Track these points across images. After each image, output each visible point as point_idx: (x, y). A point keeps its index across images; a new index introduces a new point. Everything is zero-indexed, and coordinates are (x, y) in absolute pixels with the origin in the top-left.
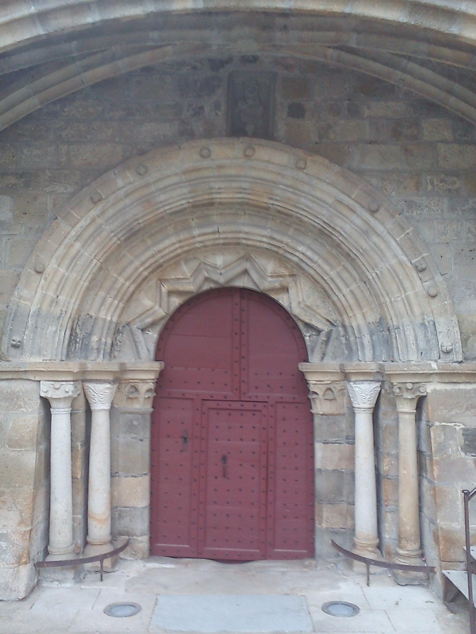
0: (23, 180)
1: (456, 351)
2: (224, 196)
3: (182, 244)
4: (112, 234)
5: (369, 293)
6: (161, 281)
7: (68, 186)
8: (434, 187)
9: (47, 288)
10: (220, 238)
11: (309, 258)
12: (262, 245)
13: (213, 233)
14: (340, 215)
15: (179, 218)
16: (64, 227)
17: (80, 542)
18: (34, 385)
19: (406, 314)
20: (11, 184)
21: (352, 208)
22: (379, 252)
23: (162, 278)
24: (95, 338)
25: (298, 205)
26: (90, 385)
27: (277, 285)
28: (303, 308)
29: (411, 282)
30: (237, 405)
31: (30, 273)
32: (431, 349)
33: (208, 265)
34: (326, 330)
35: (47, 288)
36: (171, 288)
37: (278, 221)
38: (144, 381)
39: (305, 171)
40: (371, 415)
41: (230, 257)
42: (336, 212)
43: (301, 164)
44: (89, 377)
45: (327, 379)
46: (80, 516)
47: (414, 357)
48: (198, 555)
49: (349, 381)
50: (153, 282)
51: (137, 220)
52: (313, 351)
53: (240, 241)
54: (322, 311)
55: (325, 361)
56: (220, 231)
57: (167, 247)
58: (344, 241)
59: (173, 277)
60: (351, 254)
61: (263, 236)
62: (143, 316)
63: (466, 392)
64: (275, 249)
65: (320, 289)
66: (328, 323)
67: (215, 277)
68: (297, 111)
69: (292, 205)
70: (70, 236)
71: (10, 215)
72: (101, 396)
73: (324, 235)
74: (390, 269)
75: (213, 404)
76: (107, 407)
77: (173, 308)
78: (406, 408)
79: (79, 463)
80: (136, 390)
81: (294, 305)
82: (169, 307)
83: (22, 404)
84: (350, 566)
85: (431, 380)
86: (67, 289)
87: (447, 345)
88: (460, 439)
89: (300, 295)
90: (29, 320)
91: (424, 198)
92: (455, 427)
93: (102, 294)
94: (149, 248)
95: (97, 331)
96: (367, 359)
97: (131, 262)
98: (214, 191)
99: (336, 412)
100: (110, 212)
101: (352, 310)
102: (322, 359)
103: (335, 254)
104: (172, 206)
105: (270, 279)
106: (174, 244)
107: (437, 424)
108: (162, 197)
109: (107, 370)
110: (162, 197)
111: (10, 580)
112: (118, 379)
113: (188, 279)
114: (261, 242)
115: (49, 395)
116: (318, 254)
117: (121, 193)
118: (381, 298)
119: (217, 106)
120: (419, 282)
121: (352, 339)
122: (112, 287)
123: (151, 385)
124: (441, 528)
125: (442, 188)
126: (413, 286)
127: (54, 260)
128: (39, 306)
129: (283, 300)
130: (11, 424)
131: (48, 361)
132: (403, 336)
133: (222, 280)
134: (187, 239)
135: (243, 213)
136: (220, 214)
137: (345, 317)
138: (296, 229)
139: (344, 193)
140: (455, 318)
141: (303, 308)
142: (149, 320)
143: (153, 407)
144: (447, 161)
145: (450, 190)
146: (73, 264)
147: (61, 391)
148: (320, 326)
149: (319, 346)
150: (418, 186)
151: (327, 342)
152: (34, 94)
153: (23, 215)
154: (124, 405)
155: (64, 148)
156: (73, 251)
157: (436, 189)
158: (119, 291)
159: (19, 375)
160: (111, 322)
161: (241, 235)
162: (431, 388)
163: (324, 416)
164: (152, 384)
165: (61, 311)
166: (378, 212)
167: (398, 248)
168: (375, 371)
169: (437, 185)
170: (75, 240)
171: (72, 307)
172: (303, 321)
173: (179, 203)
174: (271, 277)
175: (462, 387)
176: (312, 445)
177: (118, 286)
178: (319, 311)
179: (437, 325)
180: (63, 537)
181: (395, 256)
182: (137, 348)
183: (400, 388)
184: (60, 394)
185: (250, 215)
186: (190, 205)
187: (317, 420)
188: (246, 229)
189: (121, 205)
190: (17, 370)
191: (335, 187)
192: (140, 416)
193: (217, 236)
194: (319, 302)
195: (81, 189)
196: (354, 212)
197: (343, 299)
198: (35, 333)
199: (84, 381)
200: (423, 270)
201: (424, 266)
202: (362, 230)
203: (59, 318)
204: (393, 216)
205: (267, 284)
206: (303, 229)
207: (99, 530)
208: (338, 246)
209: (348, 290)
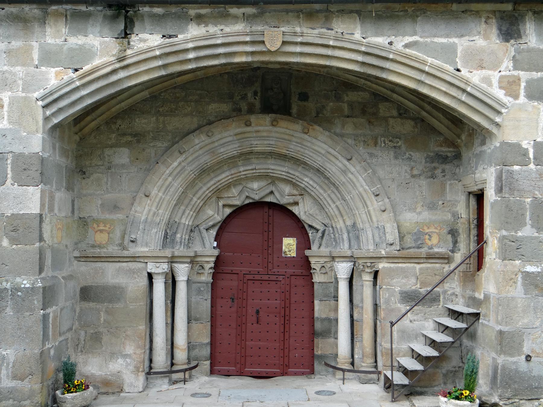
3: (233, 176)
6: (219, 198)
12: (282, 176)
13: (252, 170)
15: (231, 161)
16: (161, 168)
17: (169, 363)
18: (143, 265)
24: (179, 236)
26: (176, 265)
27: (291, 201)
29: (371, 202)
30: (266, 277)
32: (382, 243)
36: (225, 203)
38: (208, 262)
41: (263, 183)
45: (322, 260)
46: (170, 347)
47: (371, 247)
48: (241, 374)
49: (335, 262)
50: (214, 199)
52: (313, 243)
53: (269, 174)
54: (319, 217)
55: (322, 248)
57: (224, 178)
62: (207, 221)
63: (402, 268)
67: (253, 196)
68: (304, 97)
71: (128, 160)
72: (182, 271)
75: (251, 277)
76: (185, 278)
78: (368, 278)
79: (169, 314)
80: (203, 268)
81: (302, 213)
82: (223, 215)
84: (334, 375)
86: (164, 206)
88: (398, 296)
89: (306, 207)
93: (183, 208)
94: (212, 179)
95: (180, 230)
96: (345, 248)
97: (201, 188)
99: (327, 281)
100: (190, 159)
102: (319, 247)
105: (287, 197)
106: (228, 176)
107: (384, 287)
108: (222, 150)
110: (222, 150)
111: (134, 381)
112: (193, 261)
116: (316, 183)
118: (353, 211)
119: (255, 93)
120: (375, 202)
121: (337, 235)
123: (212, 265)
124: (384, 348)
126: (372, 205)
127: (156, 188)
129: (295, 210)
133: (257, 198)
134: (235, 174)
137: (333, 221)
138: (303, 167)
140: (395, 225)
142: (211, 223)
145: (395, 147)
148: (318, 227)
149: (317, 239)
150: (376, 144)
151: (322, 237)
155: (161, 119)
156: (167, 183)
157: (387, 146)
159: (134, 258)
160: (188, 225)
161: (269, 171)
162: (381, 266)
167: (363, 181)
171: (167, 217)
172: (307, 224)
174: (288, 196)
175: (400, 265)
176: (313, 302)
177: (193, 203)
178: (317, 217)
180: (161, 359)
181: (362, 186)
182: (203, 241)
183: (363, 266)
184: (159, 270)
185: (275, 158)
187: (316, 286)
188: (272, 167)
193: (254, 171)
194: (317, 212)
195: (173, 145)
198: (144, 233)
199: (172, 262)
200: (377, 195)
201: (378, 193)
203: (159, 224)
207: (181, 355)
208: (328, 179)
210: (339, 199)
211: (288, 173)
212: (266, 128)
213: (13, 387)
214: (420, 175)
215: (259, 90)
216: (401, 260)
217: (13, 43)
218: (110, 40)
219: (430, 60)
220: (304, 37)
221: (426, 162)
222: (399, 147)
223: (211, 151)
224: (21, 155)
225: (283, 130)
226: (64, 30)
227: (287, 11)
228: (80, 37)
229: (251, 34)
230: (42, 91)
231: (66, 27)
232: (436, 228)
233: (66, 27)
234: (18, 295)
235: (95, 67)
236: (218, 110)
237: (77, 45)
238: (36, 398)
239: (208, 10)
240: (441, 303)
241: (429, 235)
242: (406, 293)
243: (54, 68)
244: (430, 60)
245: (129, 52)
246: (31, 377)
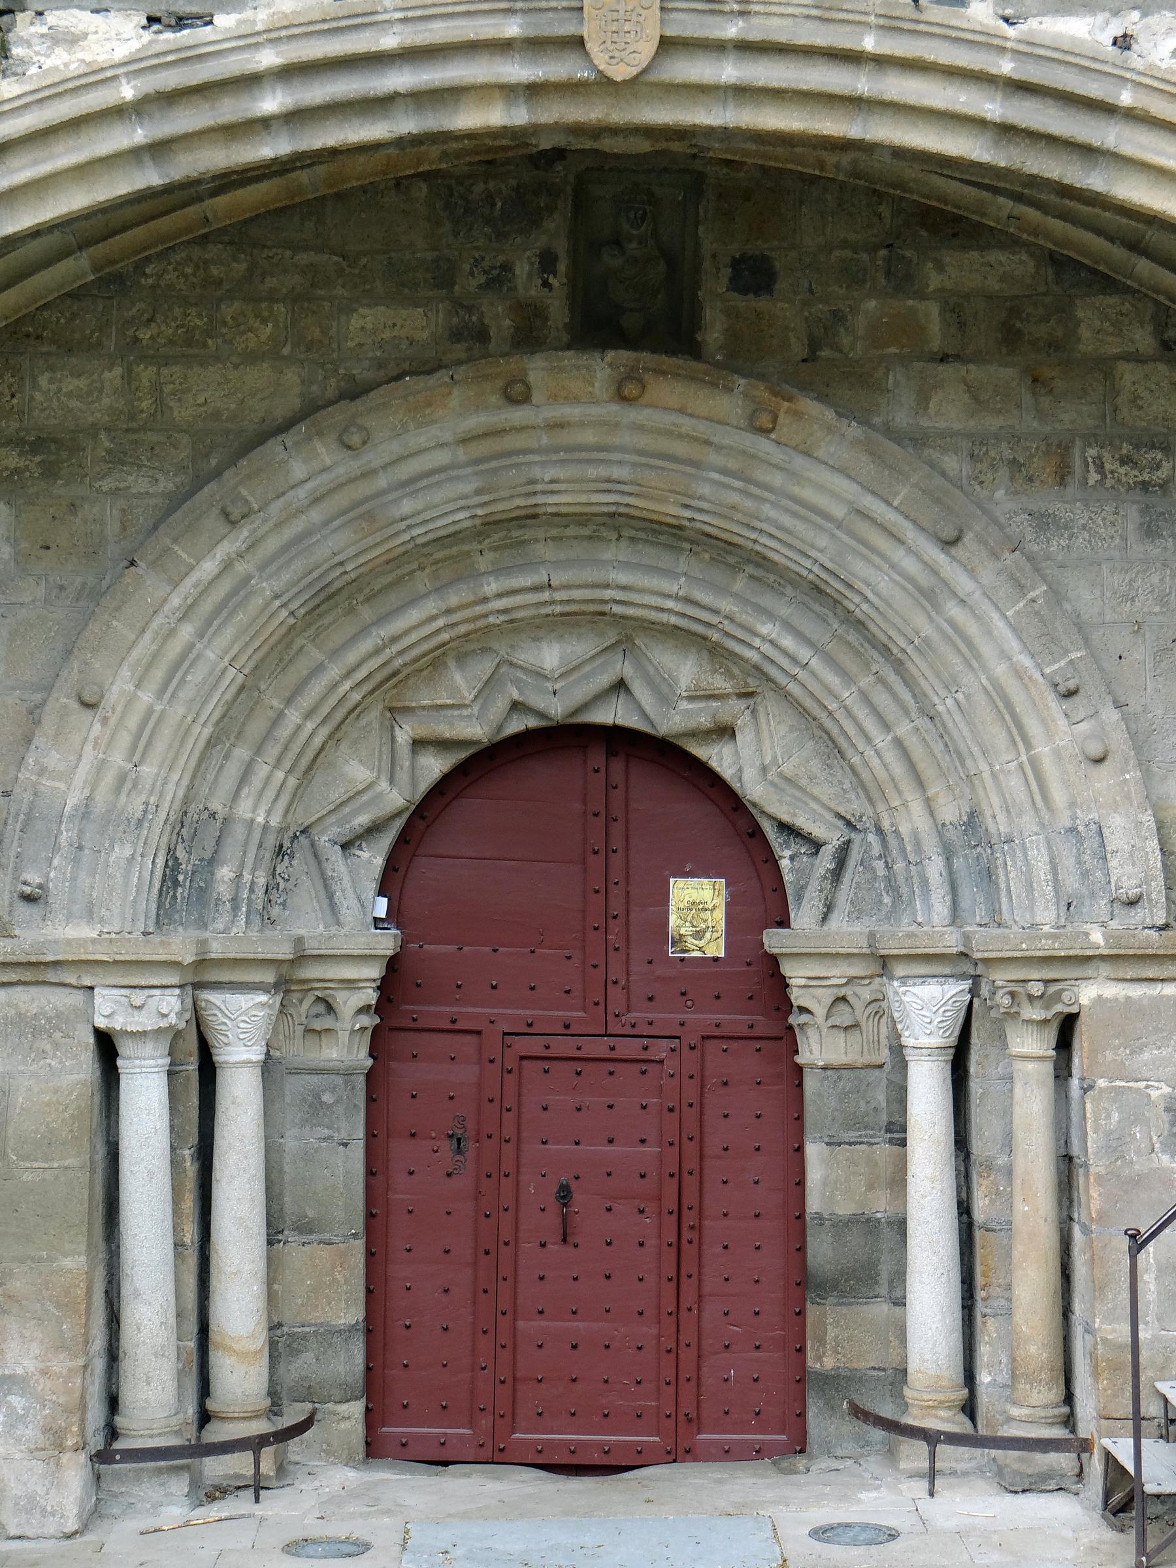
0: (38, 459)
1: (1150, 900)
2: (564, 500)
4: (277, 603)
5: (941, 746)
6: (395, 712)
7: (160, 476)
8: (1104, 477)
9: (109, 744)
10: (553, 602)
11: (786, 653)
12: (664, 617)
13: (537, 589)
14: (861, 548)
15: (445, 555)
17: (191, 1410)
18: (78, 998)
19: (1028, 806)
20: (7, 469)
21: (895, 530)
22: (964, 649)
23: (394, 704)
24: (225, 873)
25: (759, 525)
26: (214, 997)
27: (705, 721)
28: (772, 783)
30: (598, 1047)
31: (66, 706)
32: (1093, 895)
33: (521, 667)
34: (835, 842)
35: (109, 744)
36: (423, 732)
37: (707, 556)
38: (350, 984)
39: (773, 436)
40: (949, 1067)
41: (581, 647)
42: (853, 543)
43: (764, 420)
44: (213, 976)
45: (838, 972)
46: (192, 1344)
48: (495, 1454)
49: (891, 978)
51: (341, 564)
52: (799, 898)
54: (824, 792)
56: (552, 583)
58: (874, 615)
59: (426, 702)
60: (891, 646)
61: (668, 596)
62: (347, 810)
64: (699, 629)
65: (818, 733)
66: (840, 823)
67: (538, 701)
68: (754, 276)
69: (738, 522)
70: (167, 607)
72: (243, 1026)
74: (990, 688)
75: (535, 1046)
76: (256, 1054)
77: (423, 787)
78: (1031, 1045)
79: (190, 1203)
80: (330, 1009)
81: (750, 775)
83: (48, 1047)
84: (891, 1455)
85: (1090, 973)
86: (160, 746)
89: (767, 745)
90: (63, 828)
91: (1078, 504)
92: (1148, 1091)
93: (242, 753)
94: (364, 630)
95: (231, 850)
96: (936, 920)
97: (320, 668)
98: (539, 487)
99: (860, 1061)
100: (272, 544)
101: (900, 792)
102: (825, 918)
103: (856, 644)
104: (431, 526)
105: (684, 705)
106: (433, 618)
107: (1102, 1083)
109: (260, 956)
111: (40, 1490)
112: (288, 980)
113: (465, 706)
114: (662, 610)
115: (117, 1024)
116: (810, 643)
118: (969, 762)
119: (547, 262)
120: (1062, 722)
121: (899, 866)
122: (268, 735)
123: (370, 996)
124: (1105, 1341)
125: (1124, 480)
126: (1049, 735)
127: (125, 672)
128: (87, 792)
129: (720, 759)
130: (20, 1100)
131: (113, 936)
133: (557, 709)
135: (614, 536)
136: (553, 539)
137: (881, 807)
138: (751, 577)
139: (873, 493)
140: (1148, 818)
141: (772, 783)
142: (363, 820)
143: (371, 1055)
144: (1140, 408)
145: (1145, 486)
146: (175, 682)
147: (145, 1012)
148: (817, 831)
149: (814, 884)
150: (1063, 475)
151: (837, 874)
152: (80, 248)
153: (43, 552)
154: (299, 1052)
155: (146, 374)
156: (174, 648)
157: (1109, 482)
158: (286, 748)
159: (36, 970)
160: (266, 827)
161: (608, 594)
162: (1089, 993)
163: (829, 1073)
164: (370, 991)
165: (146, 804)
166: (960, 544)
168: (954, 951)
169: (1112, 472)
170: (180, 620)
171: (174, 792)
172: (771, 817)
173: (449, 520)
174: (691, 698)
176: (800, 1150)
177: (283, 733)
178: (816, 791)
181: (1005, 656)
182: (330, 896)
183: (1013, 995)
185: (632, 539)
186: (478, 522)
187: (811, 1083)
188: (623, 578)
189: (298, 526)
190: (33, 959)
191: (849, 477)
192: (340, 1080)
193: (546, 596)
194: (815, 766)
196: (901, 542)
197: (875, 762)
198: (76, 861)
199: (198, 986)
200: (1070, 694)
201: (1071, 684)
202: (919, 589)
203: (140, 823)
204: (995, 556)
205: (677, 718)
206: (772, 578)
207: (240, 1379)
208: (860, 625)
209: (889, 738)
212: (595, 411)
236: (387, 335)
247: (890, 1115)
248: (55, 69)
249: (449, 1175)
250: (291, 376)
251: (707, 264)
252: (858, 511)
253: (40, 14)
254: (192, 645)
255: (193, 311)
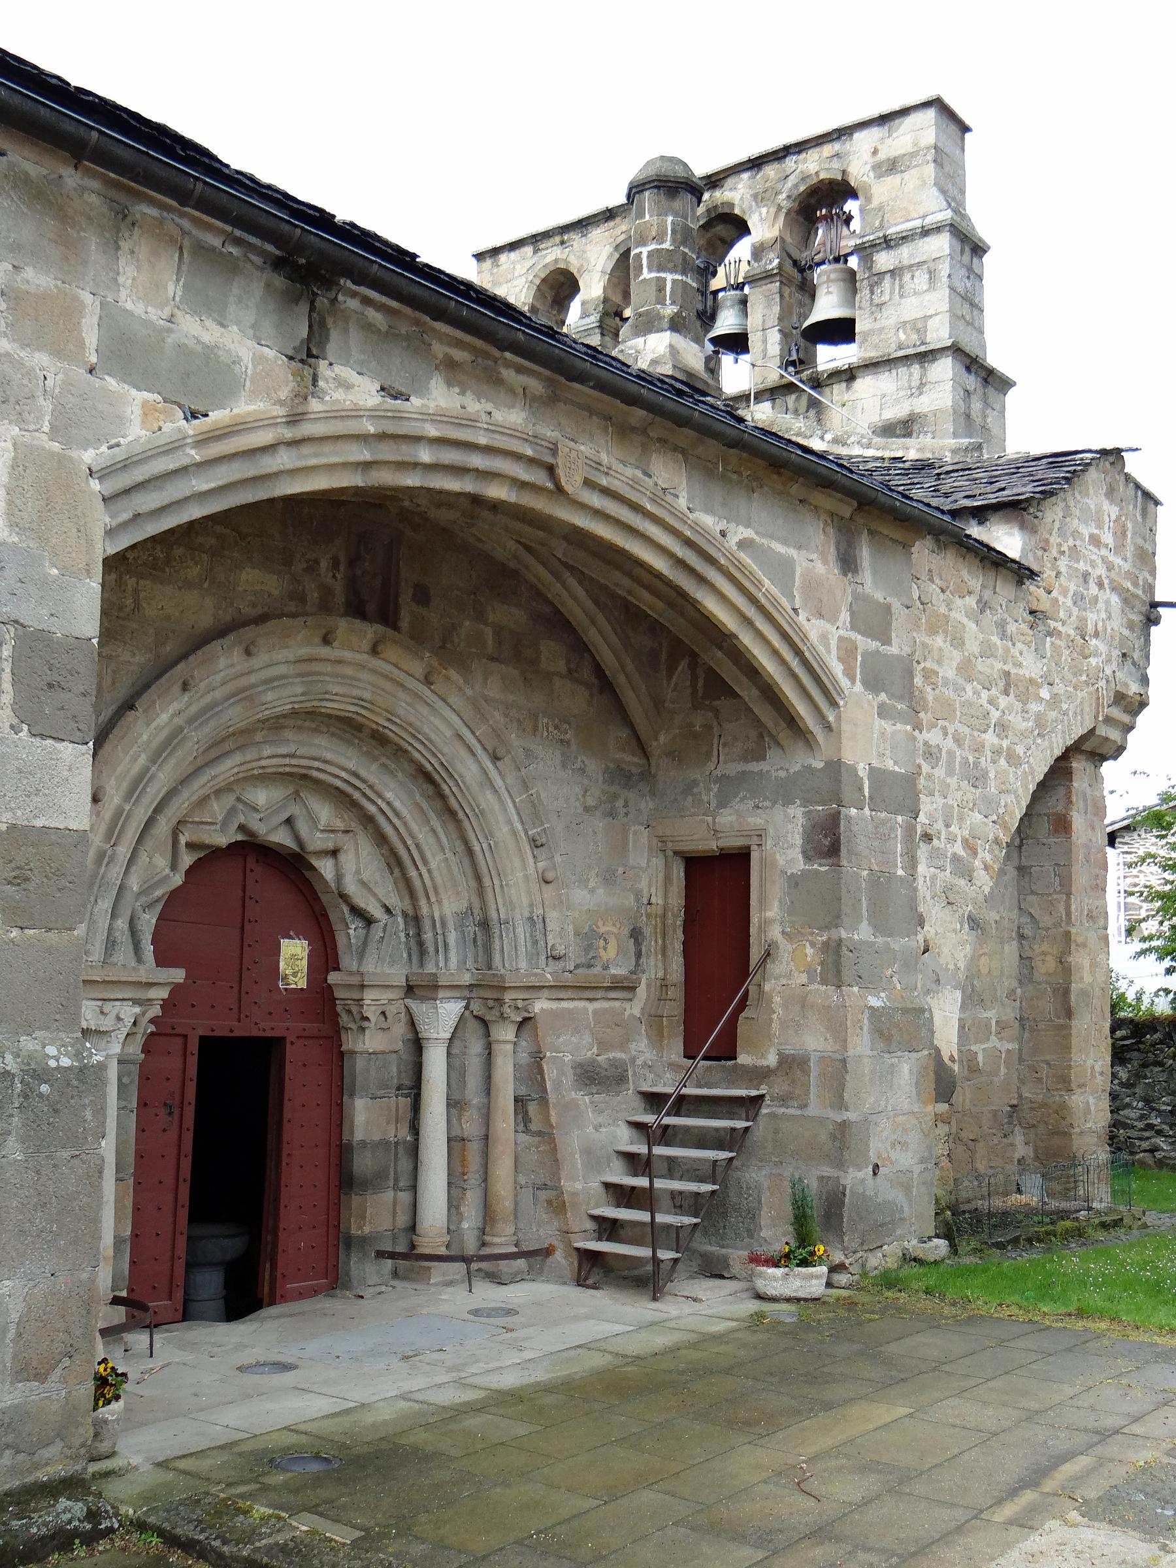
67: (303, 828)
68: (422, 596)
73: (429, 782)
87: (560, 950)
107: (548, 1054)
108: (270, 696)
117: (218, 678)
119: (335, 564)
120: (531, 860)
126: (524, 867)
132: (511, 935)
155: (131, 582)
162: (540, 1006)
178: (376, 891)
179: (547, 921)
181: (509, 822)
201: (544, 841)
210: (443, 849)
211: (356, 775)
212: (358, 656)
213: (17, 1407)
214: (596, 808)
215: (342, 558)
216: (569, 994)
217: (29, 273)
218: (276, 358)
219: (766, 582)
220: (609, 479)
221: (604, 781)
222: (568, 742)
223: (244, 695)
224: (43, 636)
225: (388, 668)
226: (171, 287)
227: (591, 411)
228: (209, 323)
229: (534, 439)
230: (104, 448)
231: (178, 280)
232: (614, 925)
233: (178, 280)
234: (41, 1095)
235: (239, 420)
236: (258, 588)
237: (199, 342)
238: (81, 1430)
239: (465, 354)
240: (631, 1086)
241: (605, 940)
242: (580, 1065)
243: (139, 390)
244: (766, 582)
245: (315, 405)
246: (66, 1362)
247: (399, 1078)
248: (337, 401)
249: (164, 1130)
250: (209, 602)
251: (403, 584)
252: (459, 735)
253: (331, 364)
254: (147, 769)
255: (158, 547)
